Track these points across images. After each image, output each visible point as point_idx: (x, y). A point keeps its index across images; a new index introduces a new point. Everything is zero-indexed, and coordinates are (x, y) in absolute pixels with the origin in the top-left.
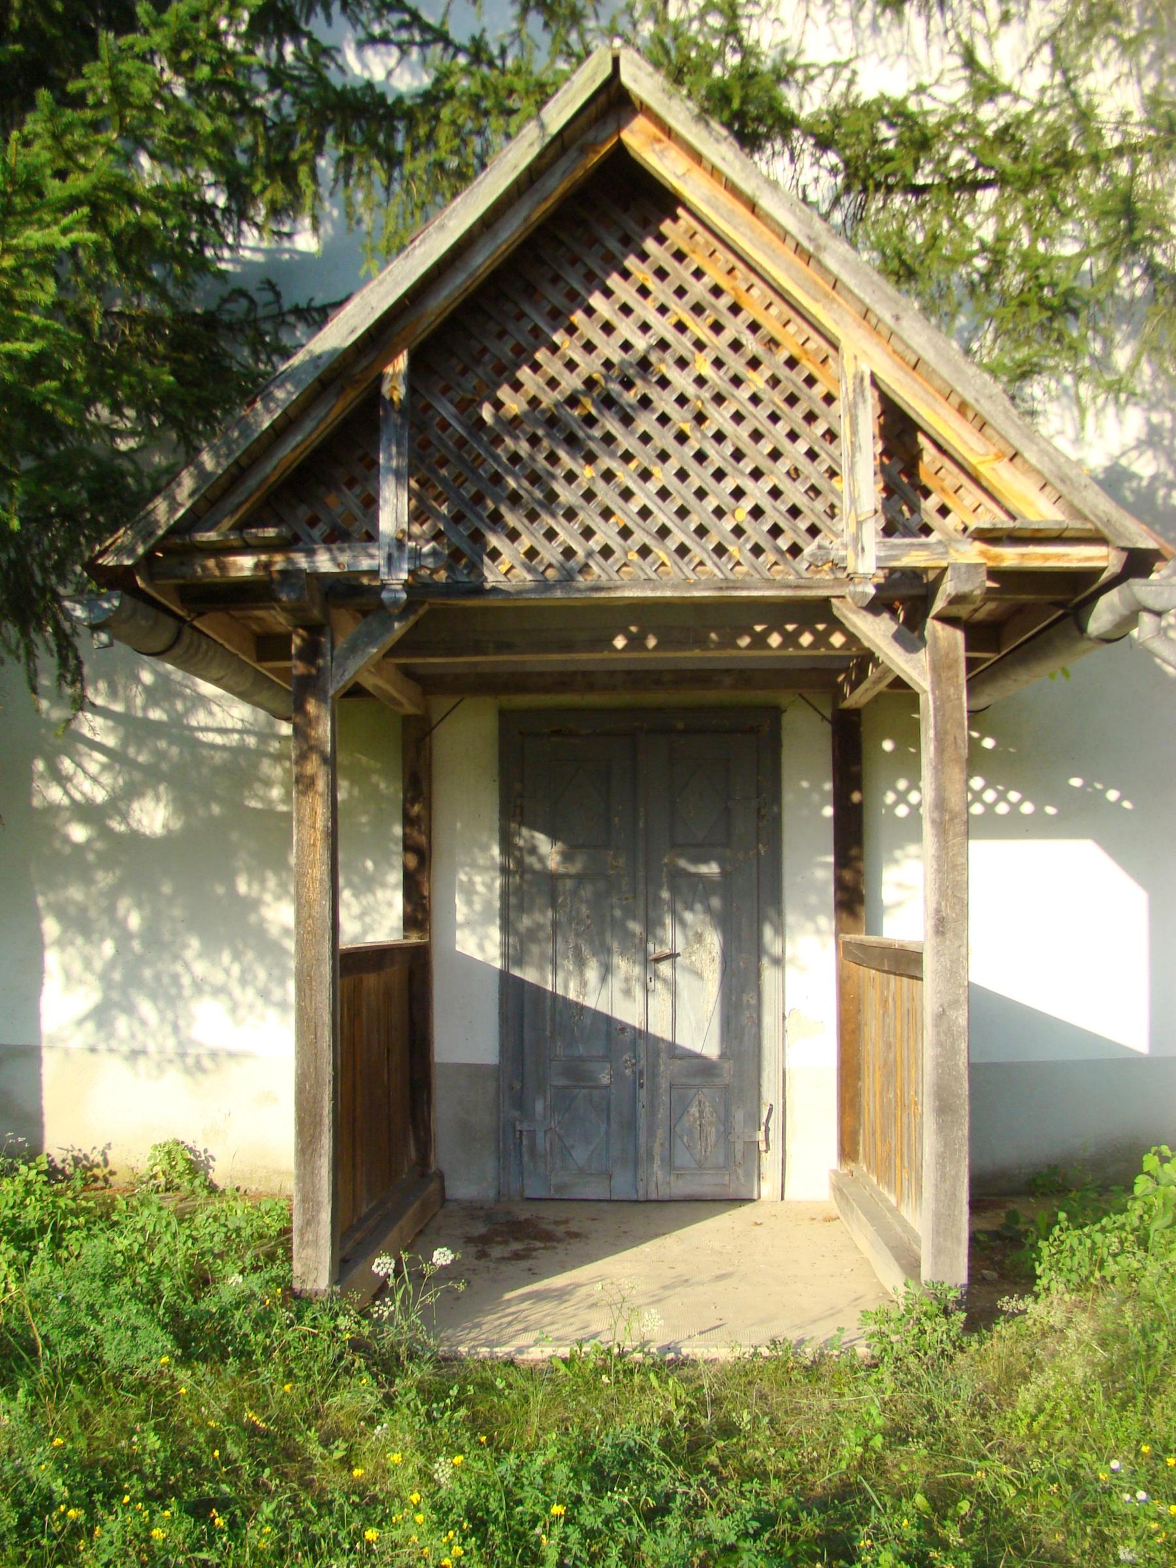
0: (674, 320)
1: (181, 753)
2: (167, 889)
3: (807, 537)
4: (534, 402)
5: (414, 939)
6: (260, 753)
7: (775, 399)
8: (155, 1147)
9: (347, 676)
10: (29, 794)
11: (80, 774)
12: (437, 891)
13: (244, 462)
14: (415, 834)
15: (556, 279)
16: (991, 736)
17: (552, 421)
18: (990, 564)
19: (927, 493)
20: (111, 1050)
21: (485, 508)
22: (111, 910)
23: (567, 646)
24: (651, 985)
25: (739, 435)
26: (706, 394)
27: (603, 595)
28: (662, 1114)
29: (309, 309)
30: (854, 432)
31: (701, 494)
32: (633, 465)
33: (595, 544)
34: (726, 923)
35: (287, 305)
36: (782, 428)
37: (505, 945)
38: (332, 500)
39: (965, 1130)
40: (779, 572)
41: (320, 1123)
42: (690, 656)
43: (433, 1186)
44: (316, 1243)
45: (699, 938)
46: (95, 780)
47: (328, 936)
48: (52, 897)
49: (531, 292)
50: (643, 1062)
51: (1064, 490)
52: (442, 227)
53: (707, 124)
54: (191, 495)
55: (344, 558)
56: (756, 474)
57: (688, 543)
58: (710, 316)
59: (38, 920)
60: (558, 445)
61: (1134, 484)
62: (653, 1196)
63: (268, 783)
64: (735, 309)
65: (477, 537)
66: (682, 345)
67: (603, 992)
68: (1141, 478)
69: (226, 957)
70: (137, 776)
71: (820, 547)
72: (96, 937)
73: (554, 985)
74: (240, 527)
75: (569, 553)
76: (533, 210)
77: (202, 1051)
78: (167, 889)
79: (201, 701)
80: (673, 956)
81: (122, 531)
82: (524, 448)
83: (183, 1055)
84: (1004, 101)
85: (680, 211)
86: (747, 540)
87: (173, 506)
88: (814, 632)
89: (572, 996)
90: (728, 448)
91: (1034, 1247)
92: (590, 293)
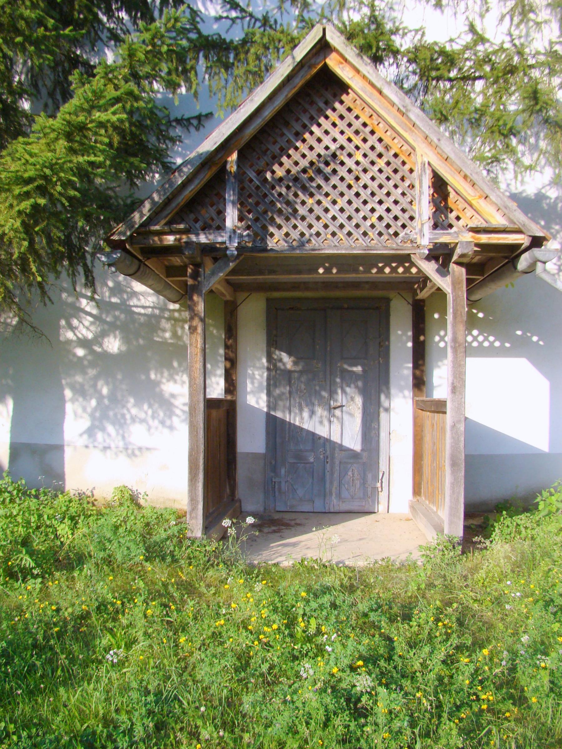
0: (347, 137)
1: (126, 317)
2: (119, 377)
3: (401, 229)
4: (288, 171)
5: (229, 397)
6: (158, 318)
7: (388, 171)
8: (115, 488)
9: (210, 285)
10: (58, 335)
11: (81, 326)
12: (239, 378)
13: (171, 197)
14: (230, 353)
15: (297, 120)
16: (482, 312)
17: (296, 179)
18: (476, 241)
19: (451, 211)
20: (95, 447)
21: (268, 216)
22: (95, 386)
23: (299, 272)
24: (332, 419)
25: (373, 186)
26: (360, 168)
27: (316, 252)
28: (336, 475)
29: (182, 119)
30: (421, 186)
31: (357, 210)
32: (329, 198)
33: (313, 231)
34: (365, 393)
35: (172, 118)
36: (391, 183)
37: (269, 402)
38: (203, 212)
39: (463, 473)
40: (390, 244)
41: (199, 469)
42: (350, 277)
43: (237, 504)
44: (196, 518)
45: (352, 399)
46: (88, 328)
47: (202, 392)
48: (69, 380)
49: (287, 124)
50: (328, 452)
51: (506, 212)
52: (252, 100)
53: (362, 58)
54: (149, 211)
55: (211, 237)
56: (380, 202)
57: (352, 231)
58: (362, 136)
59: (63, 390)
60: (298, 189)
61: (548, 201)
62: (332, 510)
63: (164, 331)
64: (372, 133)
65: (264, 228)
66: (350, 148)
67: (311, 422)
68: (551, 199)
69: (146, 407)
70: (106, 327)
71: (406, 234)
72: (88, 398)
73: (290, 419)
74: (169, 223)
75: (302, 235)
76: (289, 92)
77: (135, 447)
78: (119, 377)
79: (134, 294)
80: (342, 406)
81: (121, 225)
82: (284, 191)
83: (126, 449)
84: (487, 45)
85: (350, 91)
86: (376, 230)
87: (142, 215)
88: (404, 267)
89: (297, 423)
90: (369, 191)
91: (493, 526)
92: (312, 125)
